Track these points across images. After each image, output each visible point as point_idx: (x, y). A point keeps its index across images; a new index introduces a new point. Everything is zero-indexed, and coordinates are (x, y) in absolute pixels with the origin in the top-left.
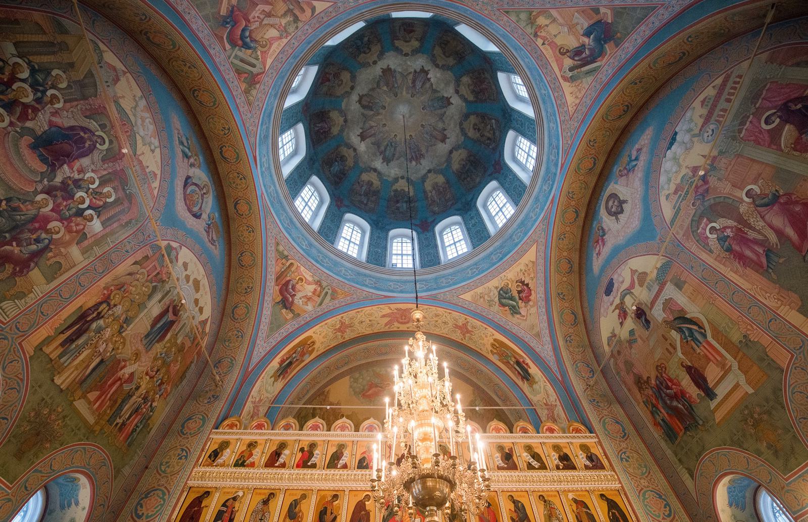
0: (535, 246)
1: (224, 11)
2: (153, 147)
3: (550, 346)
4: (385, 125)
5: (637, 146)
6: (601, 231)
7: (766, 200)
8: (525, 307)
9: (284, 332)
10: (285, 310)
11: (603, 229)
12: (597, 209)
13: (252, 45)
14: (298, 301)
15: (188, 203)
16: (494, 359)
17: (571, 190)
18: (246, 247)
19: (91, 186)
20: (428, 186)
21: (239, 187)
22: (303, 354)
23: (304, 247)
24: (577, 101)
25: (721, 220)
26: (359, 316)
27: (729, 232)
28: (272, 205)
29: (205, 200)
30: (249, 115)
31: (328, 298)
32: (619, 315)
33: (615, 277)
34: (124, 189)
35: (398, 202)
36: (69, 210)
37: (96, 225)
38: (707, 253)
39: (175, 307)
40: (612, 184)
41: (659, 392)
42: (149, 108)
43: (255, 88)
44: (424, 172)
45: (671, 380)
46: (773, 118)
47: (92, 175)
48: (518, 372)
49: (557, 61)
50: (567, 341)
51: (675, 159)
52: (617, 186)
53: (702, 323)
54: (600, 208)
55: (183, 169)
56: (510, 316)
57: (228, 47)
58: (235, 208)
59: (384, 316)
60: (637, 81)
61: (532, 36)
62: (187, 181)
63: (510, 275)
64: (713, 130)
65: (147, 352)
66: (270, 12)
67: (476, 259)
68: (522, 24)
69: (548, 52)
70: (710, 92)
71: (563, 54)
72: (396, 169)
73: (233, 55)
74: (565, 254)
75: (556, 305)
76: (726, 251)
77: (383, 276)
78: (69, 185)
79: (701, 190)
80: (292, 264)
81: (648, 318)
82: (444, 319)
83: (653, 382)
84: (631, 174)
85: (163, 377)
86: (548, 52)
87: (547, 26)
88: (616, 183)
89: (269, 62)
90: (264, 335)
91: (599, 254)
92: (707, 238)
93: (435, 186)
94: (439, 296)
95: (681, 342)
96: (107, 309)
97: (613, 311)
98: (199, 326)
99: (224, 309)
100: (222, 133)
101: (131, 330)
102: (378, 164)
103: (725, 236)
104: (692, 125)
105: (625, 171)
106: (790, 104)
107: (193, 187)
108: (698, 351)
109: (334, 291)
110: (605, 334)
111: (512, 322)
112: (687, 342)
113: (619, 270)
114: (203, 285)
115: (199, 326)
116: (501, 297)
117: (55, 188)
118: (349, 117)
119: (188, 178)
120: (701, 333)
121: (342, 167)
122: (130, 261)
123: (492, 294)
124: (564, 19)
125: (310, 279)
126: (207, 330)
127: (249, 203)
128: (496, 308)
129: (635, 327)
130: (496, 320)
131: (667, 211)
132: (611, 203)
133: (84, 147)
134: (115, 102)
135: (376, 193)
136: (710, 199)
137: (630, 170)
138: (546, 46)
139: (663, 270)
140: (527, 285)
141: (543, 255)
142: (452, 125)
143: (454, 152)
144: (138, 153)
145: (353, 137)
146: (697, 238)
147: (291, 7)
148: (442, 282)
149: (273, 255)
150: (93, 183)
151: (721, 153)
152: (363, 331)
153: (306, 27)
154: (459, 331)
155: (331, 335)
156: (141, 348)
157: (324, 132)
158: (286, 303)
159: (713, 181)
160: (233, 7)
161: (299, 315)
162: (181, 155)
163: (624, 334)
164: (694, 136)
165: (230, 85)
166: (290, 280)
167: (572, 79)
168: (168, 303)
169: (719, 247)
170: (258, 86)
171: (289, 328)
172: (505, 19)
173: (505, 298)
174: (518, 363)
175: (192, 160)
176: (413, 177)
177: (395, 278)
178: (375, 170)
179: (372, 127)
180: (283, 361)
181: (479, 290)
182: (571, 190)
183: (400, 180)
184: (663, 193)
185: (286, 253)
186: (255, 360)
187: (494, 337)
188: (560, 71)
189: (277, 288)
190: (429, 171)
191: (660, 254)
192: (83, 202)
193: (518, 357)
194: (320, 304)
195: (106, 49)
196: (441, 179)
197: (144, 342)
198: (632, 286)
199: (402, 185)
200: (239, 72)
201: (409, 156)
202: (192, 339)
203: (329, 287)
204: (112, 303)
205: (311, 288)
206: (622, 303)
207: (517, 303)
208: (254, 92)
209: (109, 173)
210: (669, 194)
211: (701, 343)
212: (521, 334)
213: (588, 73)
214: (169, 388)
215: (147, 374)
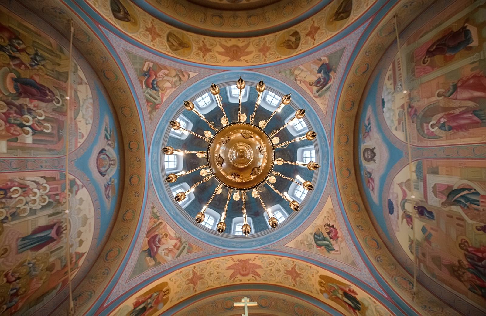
1: (145, 69)
2: (88, 122)
3: (367, 270)
5: (367, 118)
6: (368, 174)
7: (451, 91)
8: (337, 243)
9: (144, 276)
10: (149, 258)
11: (369, 173)
12: (360, 163)
13: (157, 89)
15: (99, 163)
16: (324, 298)
17: (340, 156)
19: (38, 117)
21: (135, 167)
22: (157, 302)
23: (172, 214)
24: (326, 106)
25: (433, 118)
27: (443, 120)
28: (155, 182)
29: (111, 168)
30: (150, 125)
32: (408, 223)
33: (391, 197)
34: (58, 131)
36: (15, 120)
37: (29, 139)
38: (439, 140)
39: (60, 227)
40: (362, 144)
41: (477, 269)
42: (93, 104)
43: (155, 111)
45: (478, 250)
46: (426, 60)
47: (42, 112)
48: (349, 305)
49: (309, 89)
51: (389, 109)
52: (365, 144)
53: (468, 185)
54: (361, 162)
55: (102, 143)
56: (327, 253)
57: (144, 87)
58: (130, 181)
59: (228, 268)
60: (352, 85)
61: (294, 81)
62: (102, 151)
63: (319, 221)
64: (401, 85)
65: (17, 253)
66: (168, 74)
67: (293, 220)
68: (288, 76)
69: (303, 86)
70: (389, 73)
71: (311, 85)
73: (147, 91)
74: (351, 198)
76: (449, 130)
77: (228, 239)
78: (24, 108)
79: (412, 113)
80: (161, 222)
81: (429, 210)
83: (465, 263)
84: (370, 133)
85: (20, 288)
86: (303, 86)
87: (300, 74)
88: (364, 143)
89: (165, 99)
90: (127, 276)
91: (373, 189)
92: (433, 132)
94: (270, 247)
95: (464, 211)
96: (2, 196)
97: (402, 222)
98: (74, 256)
99: (100, 254)
100: (132, 133)
101: (13, 225)
103: (443, 124)
104: (389, 91)
105: (367, 134)
106: (430, 50)
107: (105, 156)
108: (481, 208)
109: (190, 246)
110: (404, 244)
112: (468, 207)
113: (391, 191)
114: (90, 223)
115: (74, 256)
116: (316, 240)
117: (14, 105)
119: (103, 150)
120: (473, 193)
122: (42, 174)
123: (309, 239)
124: (306, 68)
125: (173, 235)
126: (81, 263)
127: (139, 177)
128: (315, 249)
129: (423, 224)
130: (317, 259)
131: (400, 135)
132: (366, 156)
133: (45, 98)
134: (75, 91)
136: (420, 113)
137: (368, 132)
138: (302, 84)
139: (419, 170)
140: (333, 226)
144: (77, 119)
146: (427, 137)
147: (178, 73)
148: (272, 239)
149: (149, 215)
150: (40, 116)
151: (411, 90)
153: (185, 84)
154: (290, 277)
155: (184, 286)
156: (14, 246)
157: (195, 165)
158: (151, 252)
159: (415, 104)
160: (150, 68)
161: (160, 263)
162: (104, 136)
163: (419, 235)
164: (393, 93)
165: (142, 107)
166: (157, 235)
167: (319, 96)
168: (55, 221)
169: (443, 131)
170: (157, 110)
171: (149, 273)
172: (280, 75)
174: (346, 294)
175: (110, 142)
177: (235, 240)
180: (137, 304)
181: (299, 238)
182: (340, 156)
184: (393, 128)
185: (158, 214)
186: (112, 298)
187: (319, 274)
188: (313, 94)
189: (147, 239)
191: (410, 161)
192: (28, 121)
193: (343, 287)
194: (178, 256)
195: (80, 69)
197: (20, 243)
198: (405, 194)
200: (148, 101)
202: (63, 264)
204: (9, 194)
205: (174, 242)
206: (404, 212)
207: (330, 242)
208: (154, 113)
209: (53, 118)
210: (396, 127)
211: (478, 201)
212: (341, 266)
213: (327, 90)
214: (20, 304)
215: (6, 276)
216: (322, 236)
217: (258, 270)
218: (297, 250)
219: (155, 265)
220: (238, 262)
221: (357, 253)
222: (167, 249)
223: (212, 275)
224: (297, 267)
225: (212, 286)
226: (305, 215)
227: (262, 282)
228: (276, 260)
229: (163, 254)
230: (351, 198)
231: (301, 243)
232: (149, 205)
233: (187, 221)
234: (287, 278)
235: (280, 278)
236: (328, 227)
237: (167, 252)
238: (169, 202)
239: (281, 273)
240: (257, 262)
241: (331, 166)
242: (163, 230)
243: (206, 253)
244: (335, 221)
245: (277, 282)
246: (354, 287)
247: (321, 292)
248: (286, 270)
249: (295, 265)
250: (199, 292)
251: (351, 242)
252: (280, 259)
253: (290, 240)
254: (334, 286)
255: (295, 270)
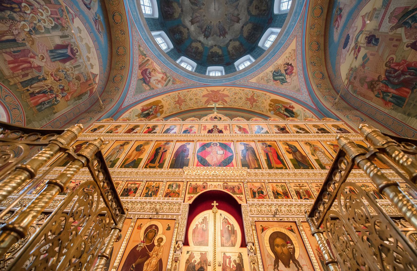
0: (295, 38)
4: (204, 16)
8: (290, 77)
9: (143, 95)
14: (153, 81)
17: (312, 61)
18: (121, 44)
20: (230, 48)
26: (189, 94)
31: (171, 82)
35: (213, 57)
44: (228, 41)
50: (318, 87)
56: (281, 85)
59: (204, 96)
72: (212, 41)
74: (315, 38)
75: (310, 69)
80: (148, 60)
82: (240, 95)
90: (132, 93)
93: (234, 48)
94: (236, 83)
102: (202, 38)
111: (284, 88)
114: (93, 52)
118: (184, 9)
121: (181, 37)
123: (269, 75)
125: (160, 71)
127: (121, 15)
128: (272, 83)
135: (201, 53)
140: (291, 65)
141: (300, 43)
142: (243, 11)
143: (245, 27)
145: (187, 22)
152: (192, 106)
154: (249, 103)
161: (153, 89)
166: (147, 69)
173: (277, 76)
176: (222, 45)
178: (200, 42)
179: (197, 17)
181: (261, 75)
183: (214, 47)
185: (145, 52)
187: (270, 99)
189: (140, 71)
190: (231, 40)
194: (166, 85)
196: (237, 43)
199: (215, 49)
201: (218, 34)
203: (171, 77)
205: (161, 76)
207: (285, 77)
215: (52, 75)
216: (280, 73)
217: (225, 98)
218: (258, 84)
219: (150, 90)
220: (211, 92)
221: (304, 83)
222: (157, 80)
223: (192, 100)
224: (255, 95)
225: (193, 108)
226: (269, 58)
227: (228, 106)
228: (240, 90)
229: (154, 83)
230: (315, 38)
231: (262, 79)
232: (136, 44)
233: (169, 62)
234: (246, 104)
235: (241, 103)
236: (286, 66)
237: (157, 82)
238: (151, 43)
239: (242, 100)
240: (226, 92)
241: (305, 5)
242: (151, 66)
243: (187, 85)
244: (294, 60)
245: (239, 107)
246: (293, 104)
247: (269, 111)
248: (247, 98)
249: (254, 94)
250: (184, 110)
251: (302, 76)
252: (243, 90)
253: (254, 77)
254: (280, 105)
255: (253, 97)
